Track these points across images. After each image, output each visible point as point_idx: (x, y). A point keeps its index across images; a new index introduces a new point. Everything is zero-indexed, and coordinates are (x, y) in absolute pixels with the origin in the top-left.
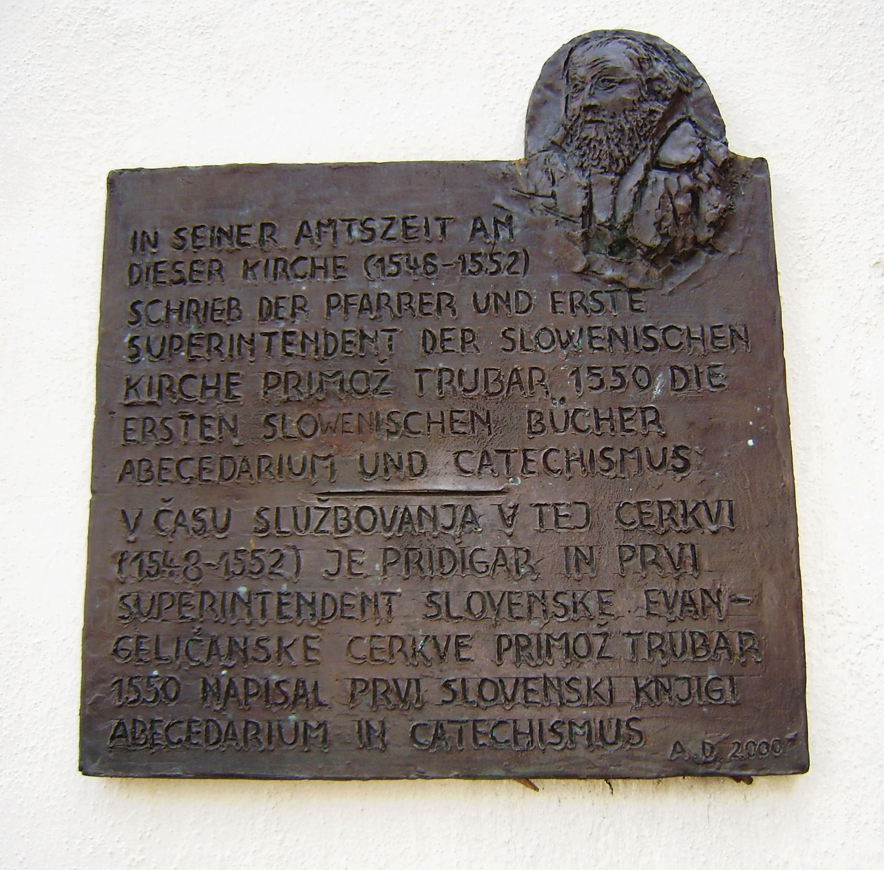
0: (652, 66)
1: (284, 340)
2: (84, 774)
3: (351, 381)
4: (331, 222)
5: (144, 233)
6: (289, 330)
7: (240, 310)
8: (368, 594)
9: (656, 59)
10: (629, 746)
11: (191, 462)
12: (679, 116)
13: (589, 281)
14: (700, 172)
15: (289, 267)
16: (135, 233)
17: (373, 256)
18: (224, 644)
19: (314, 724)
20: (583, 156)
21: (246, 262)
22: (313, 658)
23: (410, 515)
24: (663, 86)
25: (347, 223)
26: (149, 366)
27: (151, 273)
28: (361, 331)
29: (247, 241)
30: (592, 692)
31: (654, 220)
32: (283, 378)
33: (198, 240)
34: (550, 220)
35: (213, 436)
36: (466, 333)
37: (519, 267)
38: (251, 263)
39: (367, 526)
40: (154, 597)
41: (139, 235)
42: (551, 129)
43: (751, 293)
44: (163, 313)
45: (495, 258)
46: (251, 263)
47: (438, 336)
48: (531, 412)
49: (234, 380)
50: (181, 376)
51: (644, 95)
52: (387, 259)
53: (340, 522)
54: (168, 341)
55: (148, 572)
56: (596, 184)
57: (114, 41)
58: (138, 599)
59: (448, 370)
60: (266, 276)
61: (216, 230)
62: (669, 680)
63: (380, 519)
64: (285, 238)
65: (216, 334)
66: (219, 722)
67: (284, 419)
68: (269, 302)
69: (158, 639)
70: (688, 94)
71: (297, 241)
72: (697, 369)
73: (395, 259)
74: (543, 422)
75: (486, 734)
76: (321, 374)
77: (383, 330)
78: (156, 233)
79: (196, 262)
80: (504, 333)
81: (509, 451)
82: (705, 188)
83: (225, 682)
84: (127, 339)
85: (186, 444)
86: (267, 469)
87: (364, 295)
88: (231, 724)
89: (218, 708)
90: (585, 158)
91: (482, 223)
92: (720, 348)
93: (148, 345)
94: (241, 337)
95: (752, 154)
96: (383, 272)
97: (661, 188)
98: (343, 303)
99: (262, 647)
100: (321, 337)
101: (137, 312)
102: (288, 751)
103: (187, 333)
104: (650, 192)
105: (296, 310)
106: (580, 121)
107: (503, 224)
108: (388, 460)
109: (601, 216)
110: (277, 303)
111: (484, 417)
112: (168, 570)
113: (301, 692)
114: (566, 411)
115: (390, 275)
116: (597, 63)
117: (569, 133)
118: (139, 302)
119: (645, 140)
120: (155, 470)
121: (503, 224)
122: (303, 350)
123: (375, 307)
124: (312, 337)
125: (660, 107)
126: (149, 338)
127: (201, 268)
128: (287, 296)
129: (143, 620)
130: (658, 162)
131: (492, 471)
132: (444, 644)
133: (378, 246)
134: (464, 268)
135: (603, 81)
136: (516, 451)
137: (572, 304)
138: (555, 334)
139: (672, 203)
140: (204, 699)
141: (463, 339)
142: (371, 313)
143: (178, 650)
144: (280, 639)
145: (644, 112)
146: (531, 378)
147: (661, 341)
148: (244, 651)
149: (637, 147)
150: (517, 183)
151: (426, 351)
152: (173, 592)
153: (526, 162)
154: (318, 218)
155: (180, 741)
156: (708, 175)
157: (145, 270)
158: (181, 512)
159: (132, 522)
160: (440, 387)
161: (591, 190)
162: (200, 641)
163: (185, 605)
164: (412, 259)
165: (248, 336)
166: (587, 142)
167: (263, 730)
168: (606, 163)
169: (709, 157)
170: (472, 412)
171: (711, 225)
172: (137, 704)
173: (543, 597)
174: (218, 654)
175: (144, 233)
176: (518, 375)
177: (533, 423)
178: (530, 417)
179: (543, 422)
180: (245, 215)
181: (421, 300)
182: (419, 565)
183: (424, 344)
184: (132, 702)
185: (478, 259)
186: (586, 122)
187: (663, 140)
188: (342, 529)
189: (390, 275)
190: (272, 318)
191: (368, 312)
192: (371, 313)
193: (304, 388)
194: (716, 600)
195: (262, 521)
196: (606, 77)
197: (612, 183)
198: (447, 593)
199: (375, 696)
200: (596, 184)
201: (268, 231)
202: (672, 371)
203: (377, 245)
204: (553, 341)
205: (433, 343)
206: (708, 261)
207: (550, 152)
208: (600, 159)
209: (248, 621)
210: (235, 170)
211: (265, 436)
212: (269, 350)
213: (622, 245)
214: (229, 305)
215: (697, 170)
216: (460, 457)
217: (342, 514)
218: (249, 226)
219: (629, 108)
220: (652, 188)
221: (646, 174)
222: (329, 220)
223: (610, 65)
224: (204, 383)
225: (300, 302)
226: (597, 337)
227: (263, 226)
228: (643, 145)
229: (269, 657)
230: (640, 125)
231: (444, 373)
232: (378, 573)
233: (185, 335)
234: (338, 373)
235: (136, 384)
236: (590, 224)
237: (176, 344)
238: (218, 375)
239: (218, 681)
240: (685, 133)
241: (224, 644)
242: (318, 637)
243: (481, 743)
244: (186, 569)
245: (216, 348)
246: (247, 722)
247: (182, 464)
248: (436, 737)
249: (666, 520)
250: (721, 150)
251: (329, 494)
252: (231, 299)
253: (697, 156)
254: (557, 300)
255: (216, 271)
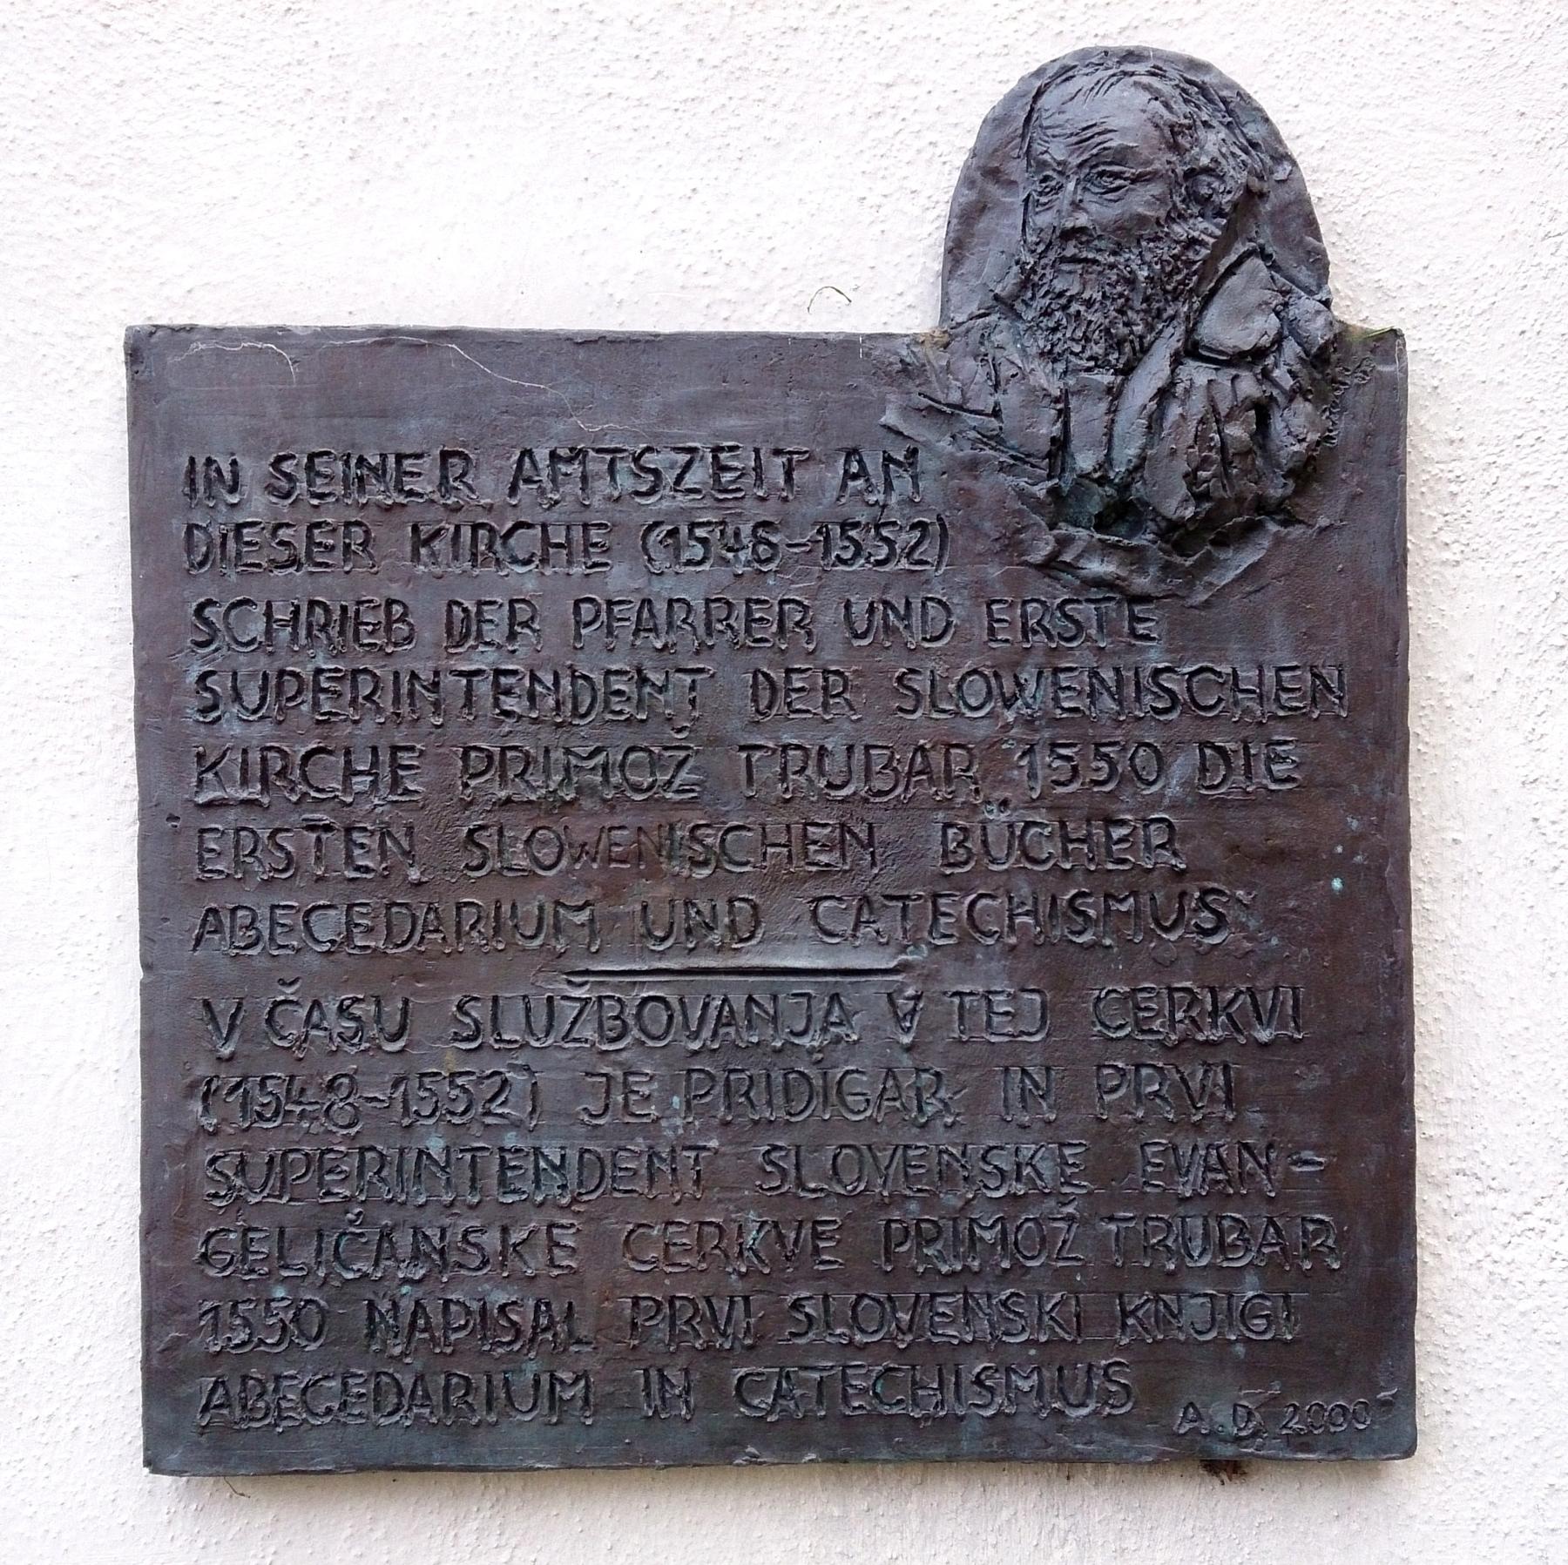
0: (1196, 142)
1: (496, 684)
2: (154, 1471)
3: (622, 766)
4: (577, 455)
5: (209, 462)
6: (503, 667)
7: (409, 624)
8: (658, 1149)
9: (1205, 123)
10: (1108, 1410)
11: (332, 912)
12: (1241, 248)
13: (1058, 579)
14: (1276, 365)
15: (499, 542)
16: (192, 461)
17: (657, 524)
18: (404, 1240)
19: (567, 1376)
20: (1054, 330)
21: (415, 529)
22: (564, 1263)
23: (731, 1011)
24: (1216, 184)
25: (608, 457)
26: (237, 729)
27: (231, 545)
28: (639, 671)
29: (417, 488)
30: (1046, 1318)
31: (1185, 468)
32: (497, 758)
33: (319, 481)
34: (987, 460)
35: (371, 865)
36: (832, 678)
37: (929, 550)
38: (425, 531)
39: (656, 1030)
40: (272, 1158)
41: (200, 467)
42: (993, 270)
43: (1354, 603)
44: (262, 626)
45: (885, 532)
46: (425, 531)
47: (781, 683)
48: (947, 826)
49: (405, 758)
50: (303, 751)
51: (1181, 206)
52: (684, 530)
53: (609, 1024)
54: (273, 682)
55: (260, 1115)
56: (1079, 392)
57: (105, 19)
58: (243, 1162)
59: (798, 747)
60: (456, 558)
61: (353, 462)
62: (1179, 1298)
63: (678, 1018)
64: (488, 486)
65: (365, 671)
66: (398, 1376)
67: (501, 833)
68: (465, 610)
69: (282, 1233)
70: (1262, 195)
71: (513, 490)
72: (1246, 749)
73: (700, 532)
74: (968, 844)
75: (865, 1391)
76: (568, 751)
77: (679, 670)
78: (234, 463)
79: (318, 525)
80: (900, 679)
81: (908, 897)
82: (1281, 399)
83: (407, 1305)
84: (192, 677)
85: (320, 879)
86: (473, 927)
87: (643, 601)
88: (420, 1378)
89: (397, 1351)
90: (1059, 335)
91: (860, 462)
92: (1291, 709)
93: (234, 688)
94: (414, 676)
95: (1379, 324)
96: (677, 557)
97: (1198, 405)
98: (604, 616)
99: (474, 1245)
100: (565, 682)
101: (206, 622)
102: (521, 1423)
103: (310, 667)
104: (1180, 410)
105: (518, 629)
106: (1052, 255)
107: (899, 464)
108: (693, 913)
109: (1085, 461)
110: (479, 613)
111: (863, 836)
112: (298, 1109)
113: (544, 1321)
114: (1011, 826)
115: (689, 563)
116: (1089, 133)
117: (1028, 282)
118: (210, 603)
119: (1175, 299)
120: (264, 927)
121: (899, 464)
122: (533, 705)
123: (663, 627)
124: (549, 679)
125: (1206, 228)
126: (235, 674)
127: (328, 531)
128: (500, 600)
129: (253, 1200)
130: (1196, 344)
131: (878, 932)
132: (793, 1235)
133: (664, 503)
134: (827, 553)
135: (1101, 174)
136: (920, 897)
137: (1024, 624)
138: (993, 681)
139: (1219, 432)
140: (371, 1335)
141: (825, 689)
142: (658, 637)
143: (319, 1251)
144: (505, 1230)
145: (1178, 242)
146: (948, 764)
147: (1183, 696)
148: (442, 1252)
149: (1160, 312)
150: (928, 382)
151: (758, 711)
152: (307, 1149)
153: (946, 339)
154: (553, 444)
155: (329, 1411)
156: (1290, 372)
157: (218, 541)
158: (316, 1004)
159: (224, 1023)
160: (784, 777)
161: (1067, 403)
162: (361, 1235)
163: (330, 1172)
164: (730, 530)
165: (426, 676)
166: (1063, 301)
167: (477, 1389)
168: (1098, 349)
169: (1294, 333)
170: (842, 825)
171: (1290, 474)
172: (247, 1349)
173: (964, 1154)
174: (393, 1256)
175: (209, 462)
176: (925, 757)
177: (952, 846)
178: (945, 835)
179: (968, 844)
180: (411, 433)
181: (749, 612)
182: (749, 1099)
183: (755, 700)
184: (237, 1346)
185: (852, 533)
186: (1063, 260)
187: (1207, 300)
188: (612, 1034)
189: (689, 563)
190: (471, 642)
191: (652, 635)
192: (658, 637)
193: (536, 779)
194: (1263, 1161)
195: (467, 1020)
196: (1105, 166)
197: (1109, 390)
198: (798, 1147)
199: (673, 1325)
200: (1079, 392)
201: (457, 465)
202: (1201, 751)
203: (665, 504)
204: (989, 692)
205: (769, 692)
206: (1278, 541)
207: (994, 318)
208: (1088, 340)
209: (447, 1198)
210: (387, 338)
211: (467, 866)
212: (469, 702)
213: (1122, 512)
214: (388, 613)
215: (1270, 361)
216: (821, 909)
217: (611, 1009)
218: (418, 456)
219: (1151, 226)
220: (1183, 403)
221: (1173, 371)
222: (571, 450)
223: (1115, 142)
224: (348, 762)
225: (523, 613)
226: (1069, 688)
227: (445, 456)
228: (1170, 311)
229: (485, 1263)
230: (1168, 269)
231: (791, 753)
232: (676, 1113)
233: (307, 672)
234: (598, 751)
235: (215, 764)
236: (1063, 470)
237: (291, 687)
238: (374, 750)
239: (395, 1305)
240: (1249, 285)
241: (404, 1240)
242: (572, 1225)
243: (856, 1404)
244: (330, 1107)
245: (368, 698)
246: (449, 1375)
247: (313, 917)
248: (778, 1394)
249: (1181, 1021)
250: (1320, 321)
251: (587, 972)
252: (390, 603)
253: (1272, 333)
254: (997, 616)
255: (359, 544)
